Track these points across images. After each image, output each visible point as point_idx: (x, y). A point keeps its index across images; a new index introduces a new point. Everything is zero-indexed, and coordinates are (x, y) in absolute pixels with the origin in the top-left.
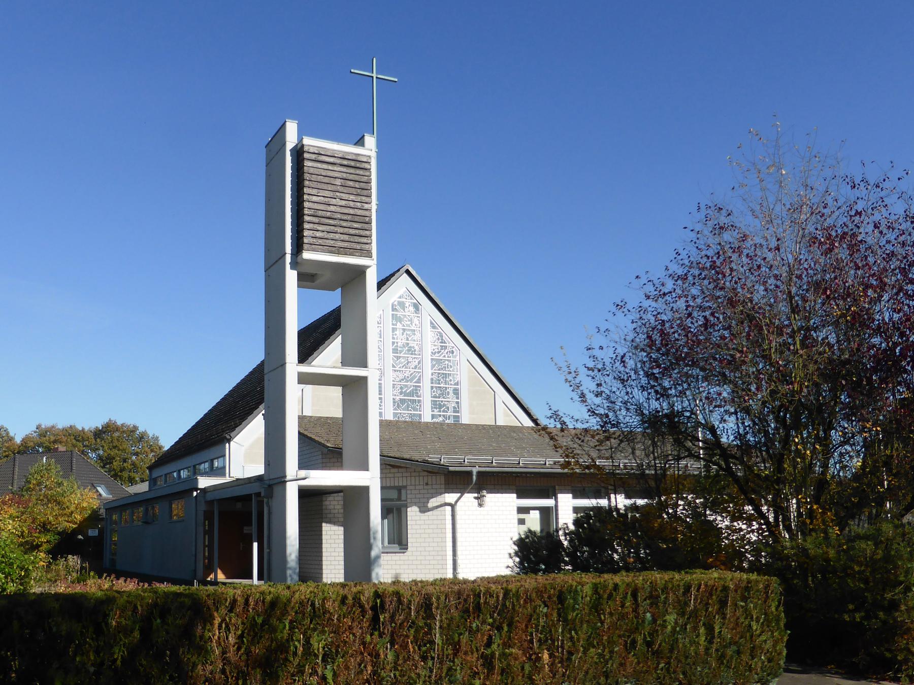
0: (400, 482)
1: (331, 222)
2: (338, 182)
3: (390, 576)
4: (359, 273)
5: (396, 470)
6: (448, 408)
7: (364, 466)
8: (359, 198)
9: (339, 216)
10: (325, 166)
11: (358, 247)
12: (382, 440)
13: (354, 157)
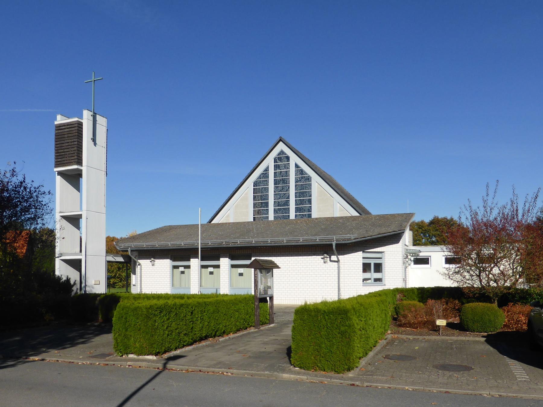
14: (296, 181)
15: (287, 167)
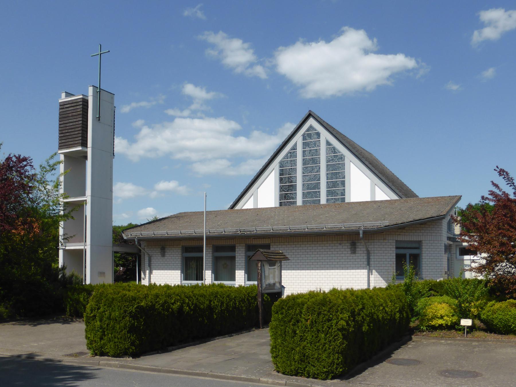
3: (167, 256)
15: (317, 144)
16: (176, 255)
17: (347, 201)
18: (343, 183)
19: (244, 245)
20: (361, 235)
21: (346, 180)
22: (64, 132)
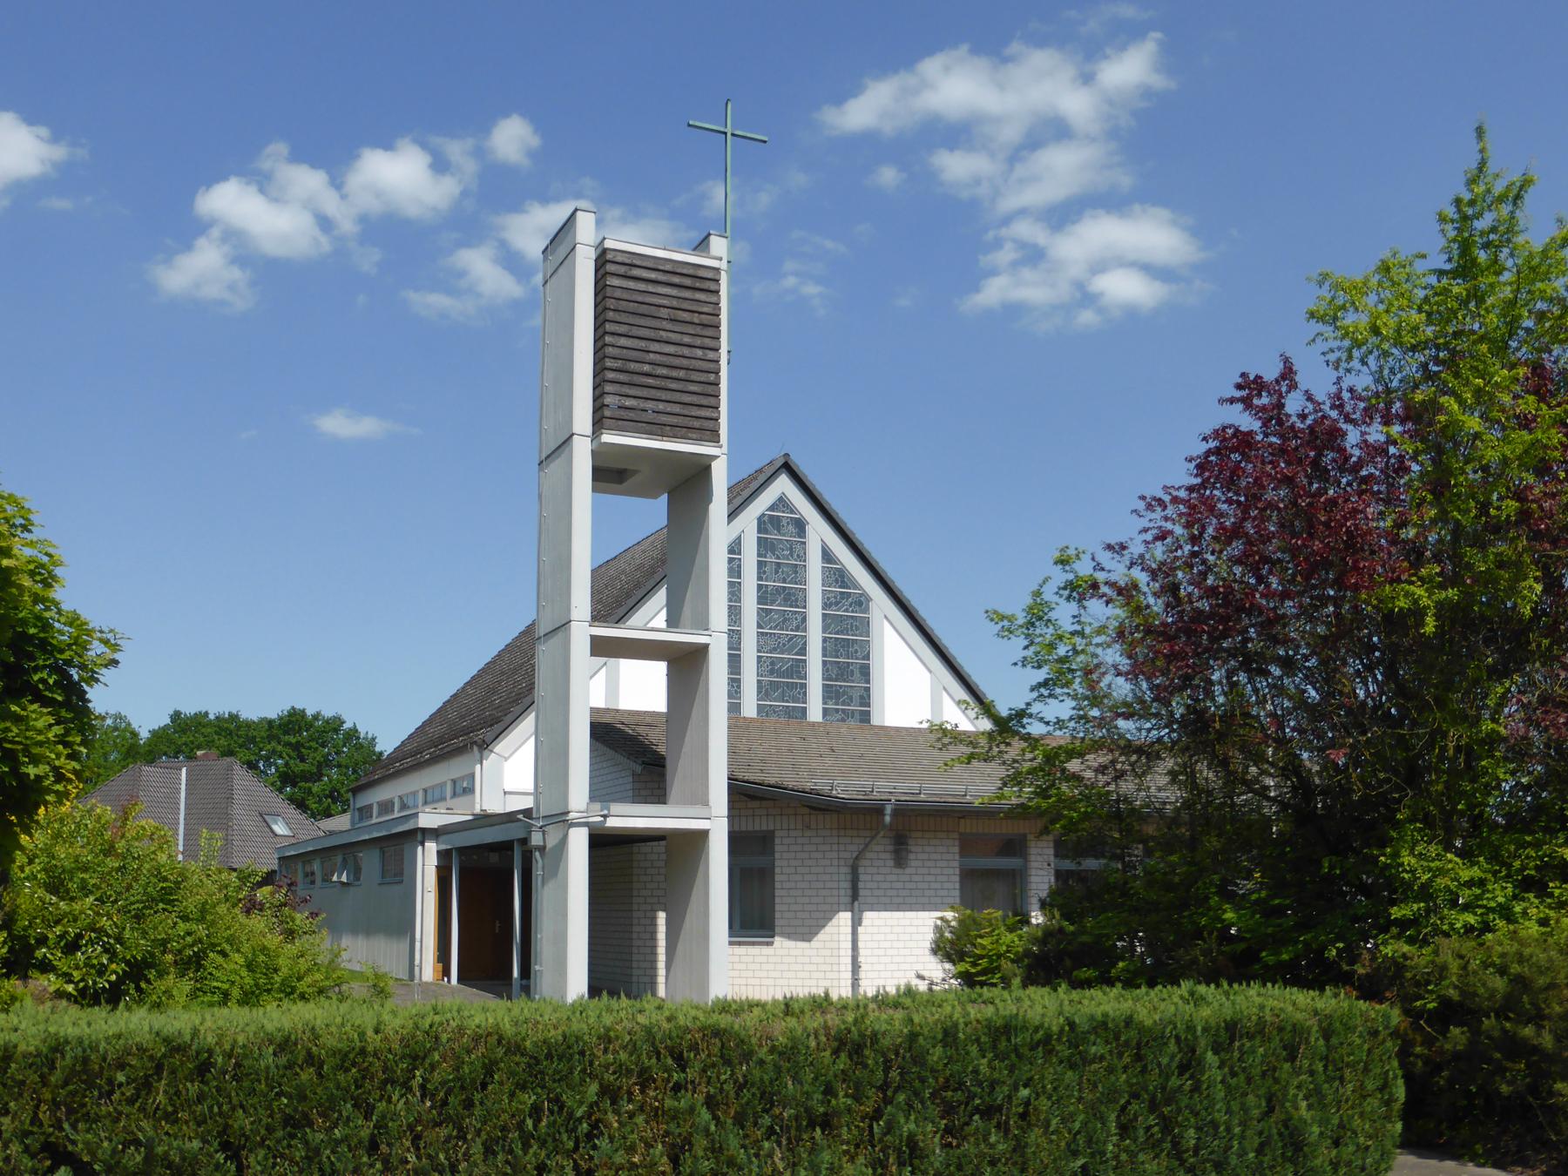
0: (761, 824)
1: (650, 381)
2: (664, 313)
3: (913, 863)
4: (700, 471)
5: (756, 804)
6: (851, 698)
7: (700, 798)
8: (698, 342)
9: (664, 371)
10: (642, 286)
11: (697, 424)
12: (733, 752)
13: (691, 271)
14: (826, 605)
15: (798, 550)
16: (940, 863)
17: (875, 721)
18: (865, 672)
19: (956, 835)
20: (888, 819)
21: (874, 663)
22: (633, 366)
